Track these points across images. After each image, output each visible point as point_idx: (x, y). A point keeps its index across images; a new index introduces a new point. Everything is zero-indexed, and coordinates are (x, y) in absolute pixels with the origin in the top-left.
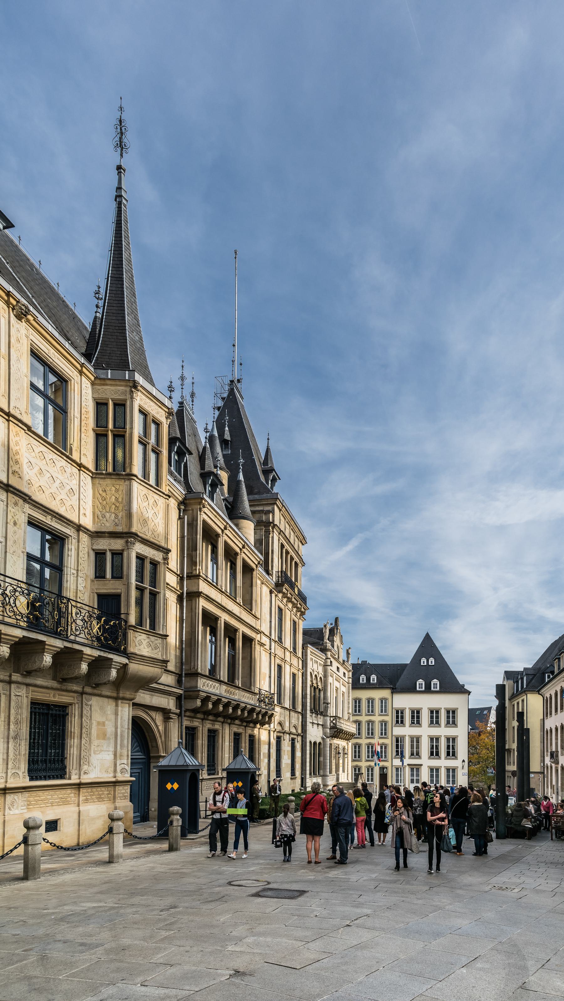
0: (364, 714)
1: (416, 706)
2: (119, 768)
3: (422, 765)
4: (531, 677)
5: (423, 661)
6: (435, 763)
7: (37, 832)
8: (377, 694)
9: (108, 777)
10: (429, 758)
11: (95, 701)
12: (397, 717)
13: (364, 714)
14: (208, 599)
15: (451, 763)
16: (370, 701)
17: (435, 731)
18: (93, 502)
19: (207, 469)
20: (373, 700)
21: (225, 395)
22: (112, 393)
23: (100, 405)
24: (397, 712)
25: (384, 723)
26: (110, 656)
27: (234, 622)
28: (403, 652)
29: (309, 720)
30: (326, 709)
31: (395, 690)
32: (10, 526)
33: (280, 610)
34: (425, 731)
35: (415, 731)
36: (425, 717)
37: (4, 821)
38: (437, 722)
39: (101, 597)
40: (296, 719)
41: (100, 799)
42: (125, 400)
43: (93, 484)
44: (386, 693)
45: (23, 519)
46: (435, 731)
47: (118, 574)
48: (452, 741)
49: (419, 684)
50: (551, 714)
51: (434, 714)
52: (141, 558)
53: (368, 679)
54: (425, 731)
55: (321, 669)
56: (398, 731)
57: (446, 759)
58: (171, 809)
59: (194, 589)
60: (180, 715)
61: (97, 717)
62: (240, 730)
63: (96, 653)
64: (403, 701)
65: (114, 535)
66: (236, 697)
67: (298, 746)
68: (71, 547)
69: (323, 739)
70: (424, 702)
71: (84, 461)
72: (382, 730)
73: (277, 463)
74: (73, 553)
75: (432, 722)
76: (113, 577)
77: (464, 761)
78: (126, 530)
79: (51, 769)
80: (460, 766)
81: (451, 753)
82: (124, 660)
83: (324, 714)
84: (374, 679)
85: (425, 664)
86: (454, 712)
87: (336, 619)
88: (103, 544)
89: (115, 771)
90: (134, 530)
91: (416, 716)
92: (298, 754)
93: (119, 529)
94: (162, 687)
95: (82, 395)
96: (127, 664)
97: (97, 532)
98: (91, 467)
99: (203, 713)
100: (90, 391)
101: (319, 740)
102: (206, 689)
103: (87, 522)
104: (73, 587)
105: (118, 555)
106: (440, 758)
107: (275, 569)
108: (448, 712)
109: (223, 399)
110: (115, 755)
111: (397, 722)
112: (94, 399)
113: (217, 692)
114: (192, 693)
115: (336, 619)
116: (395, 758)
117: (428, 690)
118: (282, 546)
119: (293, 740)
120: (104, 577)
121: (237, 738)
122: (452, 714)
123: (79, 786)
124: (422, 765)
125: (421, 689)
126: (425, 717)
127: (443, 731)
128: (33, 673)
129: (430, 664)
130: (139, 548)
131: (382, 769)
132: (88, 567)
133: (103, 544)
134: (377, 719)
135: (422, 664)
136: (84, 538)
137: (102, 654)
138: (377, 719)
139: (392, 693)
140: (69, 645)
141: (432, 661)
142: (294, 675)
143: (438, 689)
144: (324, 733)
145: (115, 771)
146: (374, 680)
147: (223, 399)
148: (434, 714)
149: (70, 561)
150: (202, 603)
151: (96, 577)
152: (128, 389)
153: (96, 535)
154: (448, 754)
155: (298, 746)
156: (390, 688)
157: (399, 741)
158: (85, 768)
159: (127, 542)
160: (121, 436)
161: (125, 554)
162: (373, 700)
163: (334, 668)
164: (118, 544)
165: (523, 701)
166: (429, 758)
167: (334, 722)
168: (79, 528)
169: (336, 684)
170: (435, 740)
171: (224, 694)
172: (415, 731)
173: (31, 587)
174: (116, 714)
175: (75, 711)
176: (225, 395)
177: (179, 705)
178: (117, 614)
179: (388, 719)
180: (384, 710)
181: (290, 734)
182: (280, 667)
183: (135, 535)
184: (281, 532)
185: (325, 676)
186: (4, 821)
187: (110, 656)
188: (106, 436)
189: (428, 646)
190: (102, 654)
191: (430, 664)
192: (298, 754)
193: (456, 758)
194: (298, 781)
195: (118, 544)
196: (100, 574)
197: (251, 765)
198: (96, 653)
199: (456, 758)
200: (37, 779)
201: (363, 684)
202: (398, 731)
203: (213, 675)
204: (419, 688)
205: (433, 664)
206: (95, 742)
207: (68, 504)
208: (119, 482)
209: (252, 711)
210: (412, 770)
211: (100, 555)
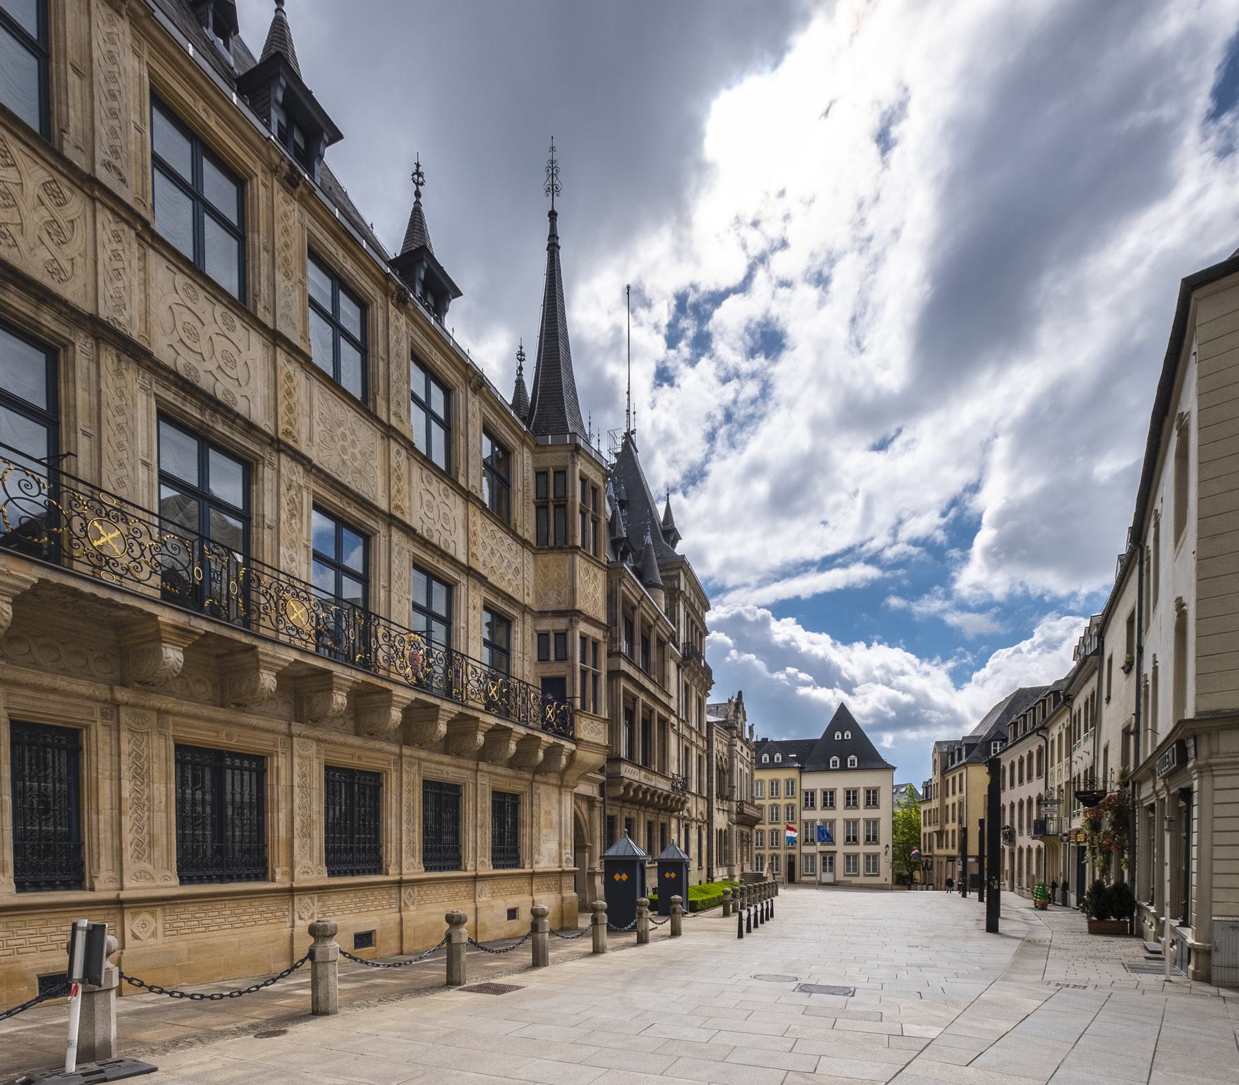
2: (564, 858)
5: (838, 735)
6: (852, 849)
8: (782, 775)
9: (554, 867)
11: (542, 790)
14: (629, 678)
17: (852, 814)
18: (535, 580)
19: (618, 535)
21: (619, 450)
22: (552, 460)
23: (541, 474)
25: (790, 808)
26: (563, 742)
27: (649, 703)
29: (715, 806)
30: (732, 792)
32: (470, 611)
33: (687, 686)
34: (840, 814)
37: (476, 909)
38: (855, 804)
39: (545, 681)
40: (702, 806)
41: (549, 889)
42: (567, 467)
43: (535, 561)
44: (793, 774)
45: (479, 603)
46: (852, 814)
47: (563, 656)
52: (584, 638)
53: (772, 759)
54: (840, 814)
55: (725, 749)
56: (807, 815)
59: (615, 668)
60: (603, 802)
61: (544, 806)
62: (653, 819)
63: (551, 740)
64: (815, 782)
65: (558, 614)
66: (653, 784)
67: (704, 834)
68: (517, 628)
70: (839, 782)
71: (527, 536)
73: (678, 522)
74: (519, 636)
75: (848, 804)
76: (556, 659)
78: (569, 608)
79: (508, 859)
80: (882, 853)
81: (872, 839)
82: (573, 747)
83: (729, 799)
84: (835, 762)
87: (740, 694)
88: (546, 625)
89: (560, 861)
90: (578, 607)
91: (829, 799)
92: (705, 843)
93: (563, 607)
95: (524, 466)
96: (574, 752)
97: (540, 612)
98: (533, 542)
99: (623, 800)
100: (530, 461)
101: (724, 827)
102: (627, 775)
103: (529, 601)
104: (520, 671)
105: (562, 636)
106: (858, 844)
107: (682, 641)
109: (617, 455)
110: (560, 845)
112: (535, 469)
113: (637, 778)
114: (614, 779)
115: (740, 694)
117: (844, 768)
118: (688, 615)
119: (700, 827)
120: (548, 660)
121: (650, 826)
122: (872, 798)
123: (532, 875)
127: (862, 814)
130: (583, 627)
131: (791, 857)
132: (532, 652)
133: (546, 625)
134: (782, 802)
136: (528, 619)
137: (556, 741)
138: (782, 802)
140: (530, 732)
142: (700, 757)
144: (730, 820)
145: (560, 861)
147: (617, 455)
148: (851, 798)
149: (517, 644)
150: (623, 683)
151: (539, 660)
152: (569, 454)
153: (543, 614)
155: (704, 834)
158: (536, 857)
159: (571, 621)
160: (562, 505)
161: (569, 634)
163: (738, 748)
164: (561, 624)
165: (954, 779)
168: (525, 609)
169: (740, 766)
170: (851, 824)
171: (643, 780)
174: (560, 803)
175: (526, 800)
176: (619, 450)
177: (602, 794)
178: (562, 698)
179: (795, 802)
180: (790, 792)
181: (697, 821)
182: (687, 749)
183: (579, 613)
184: (687, 600)
185: (731, 757)
186: (476, 909)
187: (563, 742)
188: (546, 507)
190: (556, 741)
192: (705, 843)
193: (878, 843)
194: (705, 871)
195: (561, 624)
196: (543, 657)
197: (684, 856)
198: (551, 740)
199: (878, 843)
200: (37, 887)
203: (631, 759)
206: (544, 831)
207: (514, 583)
208: (561, 556)
209: (668, 797)
210: (825, 859)
211: (542, 637)
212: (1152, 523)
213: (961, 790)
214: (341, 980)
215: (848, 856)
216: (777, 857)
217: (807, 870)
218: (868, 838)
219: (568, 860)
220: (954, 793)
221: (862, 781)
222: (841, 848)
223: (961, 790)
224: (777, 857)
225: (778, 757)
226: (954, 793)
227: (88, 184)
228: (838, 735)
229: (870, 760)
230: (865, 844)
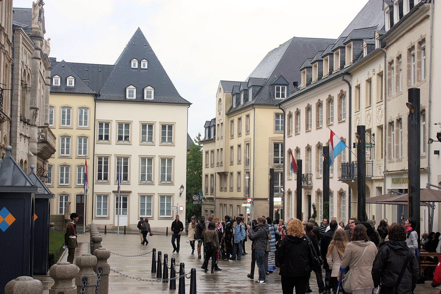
1: (124, 118)
4: (258, 89)
5: (134, 64)
6: (147, 189)
7: (66, 286)
8: (75, 102)
15: (166, 190)
20: (69, 108)
31: (97, 98)
35: (123, 150)
36: (135, 132)
44: (88, 101)
46: (147, 151)
48: (167, 161)
50: (297, 134)
51: (147, 128)
56: (102, 149)
64: (112, 113)
69: (29, 156)
72: (80, 147)
75: (143, 140)
81: (167, 178)
84: (71, 82)
85: (137, 67)
86: (170, 127)
94: (303, 90)
101: (25, 158)
106: (152, 184)
108: (164, 127)
117: (140, 100)
125: (131, 98)
126: (135, 132)
127: (157, 150)
129: (142, 67)
134: (74, 133)
138: (74, 133)
139: (96, 100)
141: (145, 64)
143: (152, 98)
144: (31, 149)
148: (147, 128)
157: (103, 162)
162: (69, 108)
167: (44, 134)
170: (147, 161)
172: (123, 150)
179: (89, 133)
180: (83, 119)
189: (139, 46)
191: (142, 67)
193: (172, 184)
199: (172, 184)
202: (102, 149)
205: (146, 67)
213: (248, 132)
215: (143, 197)
217: (99, 212)
219: (424, 157)
220: (240, 134)
221: (158, 115)
222: (135, 187)
223: (248, 132)
225: (71, 82)
226: (240, 134)
229: (168, 96)
230: (161, 184)
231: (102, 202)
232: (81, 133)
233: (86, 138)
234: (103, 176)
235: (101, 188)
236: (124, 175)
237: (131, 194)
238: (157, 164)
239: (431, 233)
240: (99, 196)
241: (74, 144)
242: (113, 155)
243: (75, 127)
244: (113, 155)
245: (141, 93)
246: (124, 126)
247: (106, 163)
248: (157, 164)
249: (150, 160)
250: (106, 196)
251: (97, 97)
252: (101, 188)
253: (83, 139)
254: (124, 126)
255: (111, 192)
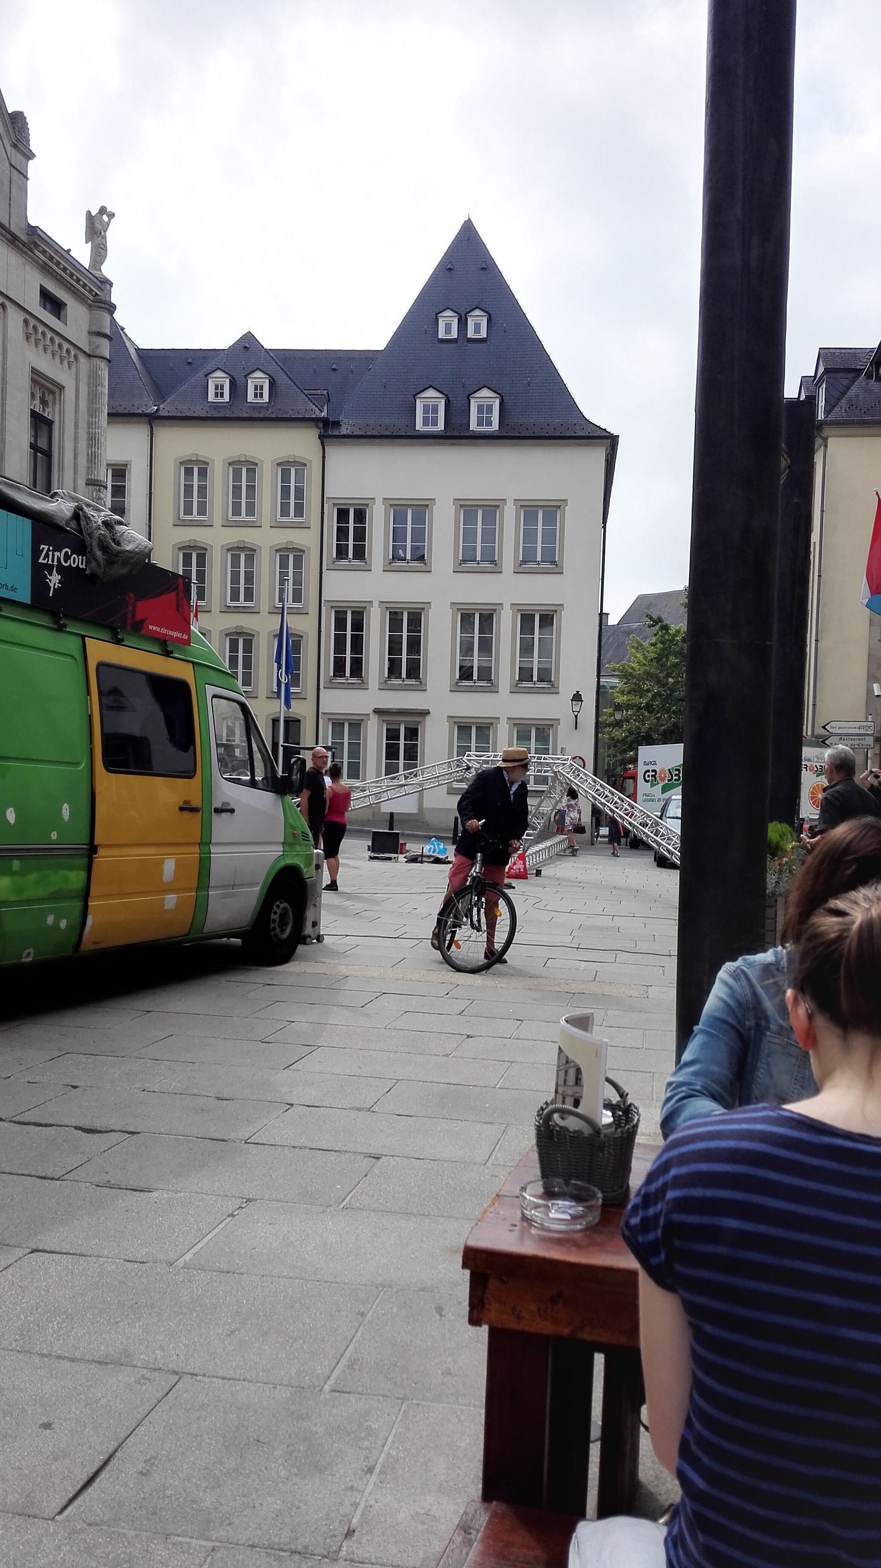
0: (218, 521)
3: (426, 713)
8: (268, 446)
10: (455, 689)
12: (342, 533)
13: (218, 521)
16: (244, 469)
20: (252, 468)
24: (342, 515)
28: (358, 310)
35: (405, 588)
44: (301, 443)
46: (478, 590)
49: (426, 409)
57: (516, 690)
58: (791, 390)
64: (365, 474)
77: (577, 697)
81: (536, 677)
85: (454, 334)
106: (493, 688)
111: (341, 552)
116: (330, 686)
117: (457, 433)
124: (426, 713)
126: (443, 536)
127: (508, 590)
128: (276, 741)
129: (471, 334)
134: (266, 538)
135: (442, 335)
138: (266, 538)
141: (478, 325)
146: (258, 394)
154: (394, 669)
156: (315, 421)
157: (350, 622)
166: (455, 689)
170: (477, 621)
173: (541, 980)
179: (307, 539)
180: (292, 502)
189: (467, 274)
191: (471, 334)
201: (215, 406)
202: (345, 586)
204: (425, 422)
205: (483, 334)
210: (392, 735)
212: (218, 941)
214: (283, 931)
216: (251, 553)
218: (525, 674)
221: (513, 475)
222: (439, 698)
224: (251, 553)
227: (352, 1109)
228: (447, 325)
231: (346, 741)
232: (283, 537)
233: (300, 554)
234: (349, 667)
235: (341, 701)
236: (406, 664)
237: (427, 718)
238: (506, 629)
239: (283, 843)
240: (338, 725)
241: (266, 569)
242: (376, 604)
243: (266, 522)
244: (376, 604)
245: (456, 414)
246: (411, 516)
247: (358, 626)
248: (506, 629)
249: (487, 619)
250: (356, 725)
251: (329, 431)
252: (341, 701)
253: (290, 557)
254: (411, 516)
255: (370, 712)
